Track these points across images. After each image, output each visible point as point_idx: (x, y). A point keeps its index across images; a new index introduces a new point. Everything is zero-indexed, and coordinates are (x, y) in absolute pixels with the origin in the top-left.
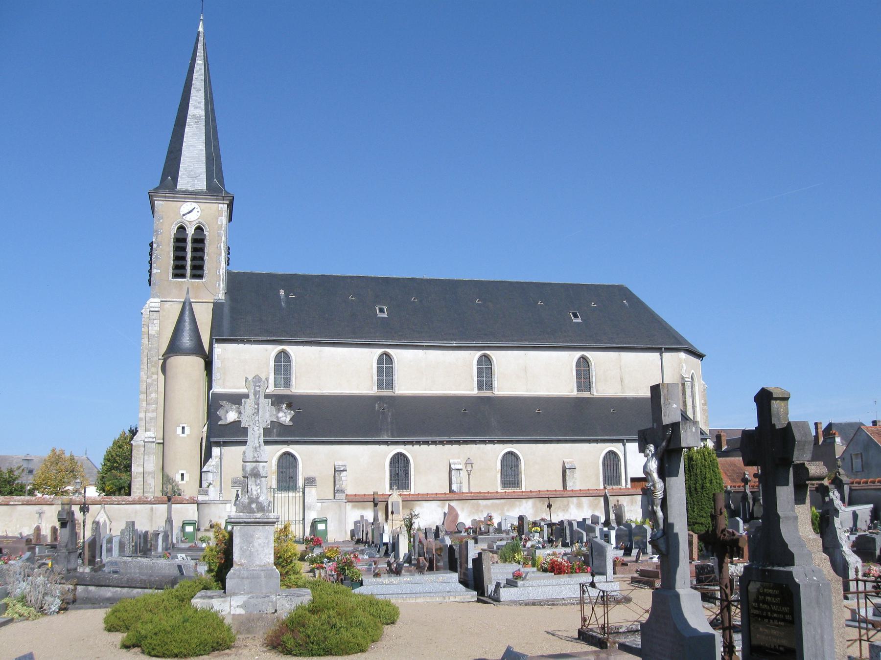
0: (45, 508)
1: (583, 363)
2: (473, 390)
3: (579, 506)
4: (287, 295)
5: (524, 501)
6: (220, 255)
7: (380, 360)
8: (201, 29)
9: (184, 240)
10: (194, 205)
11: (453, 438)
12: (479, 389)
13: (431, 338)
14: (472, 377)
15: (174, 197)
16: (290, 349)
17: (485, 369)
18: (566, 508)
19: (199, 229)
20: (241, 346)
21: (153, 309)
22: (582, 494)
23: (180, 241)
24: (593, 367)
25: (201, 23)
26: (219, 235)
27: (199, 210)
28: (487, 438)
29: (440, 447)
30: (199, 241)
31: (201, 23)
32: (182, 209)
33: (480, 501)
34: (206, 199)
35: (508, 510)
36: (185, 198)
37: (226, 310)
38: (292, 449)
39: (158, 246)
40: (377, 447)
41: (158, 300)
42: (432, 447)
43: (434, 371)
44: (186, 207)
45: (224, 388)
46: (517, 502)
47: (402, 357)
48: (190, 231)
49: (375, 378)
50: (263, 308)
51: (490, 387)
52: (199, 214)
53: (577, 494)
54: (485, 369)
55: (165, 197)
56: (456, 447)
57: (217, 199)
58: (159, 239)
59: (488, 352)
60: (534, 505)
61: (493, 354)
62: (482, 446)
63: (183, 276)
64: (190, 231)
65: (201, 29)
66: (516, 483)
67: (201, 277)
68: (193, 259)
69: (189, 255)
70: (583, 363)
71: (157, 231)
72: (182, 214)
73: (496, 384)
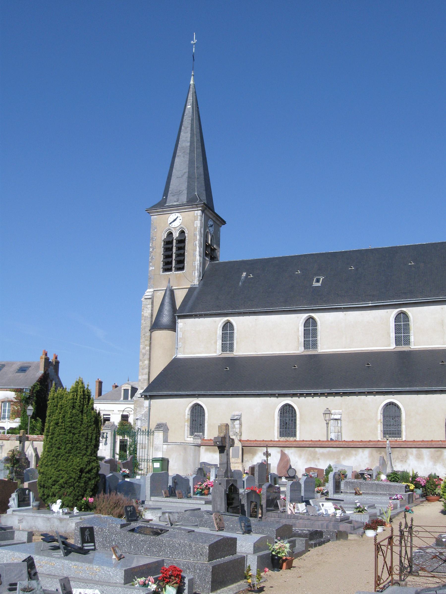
0: (5, 442)
1: (228, 327)
2: (389, 345)
3: (419, 457)
4: (247, 275)
5: (360, 450)
6: (196, 251)
7: (397, 318)
8: (192, 82)
9: (171, 243)
10: (178, 215)
11: (334, 390)
12: (396, 344)
13: (352, 300)
14: (389, 334)
15: (163, 211)
16: (233, 320)
17: (402, 326)
18: (404, 459)
19: (182, 232)
20: (197, 320)
21: (146, 297)
22: (422, 444)
23: (168, 243)
24: (319, 327)
25: (192, 77)
26: (195, 235)
27: (181, 218)
28: (312, 391)
29: (323, 398)
30: (182, 241)
31: (192, 77)
32: (169, 219)
33: (317, 449)
34: (185, 209)
35: (344, 459)
36: (171, 210)
37: (195, 293)
38: (201, 401)
39: (153, 250)
40: (268, 399)
41: (152, 290)
42: (316, 398)
43: (355, 330)
44: (172, 217)
45: (184, 354)
46: (353, 451)
47: (324, 319)
48: (176, 235)
49: (302, 339)
50: (230, 288)
51: (407, 342)
52: (181, 221)
53: (417, 445)
54: (402, 326)
55: (158, 212)
56: (338, 398)
57: (193, 208)
58: (154, 244)
59: (404, 309)
60: (371, 455)
61: (410, 311)
62: (363, 397)
63: (170, 270)
64: (176, 235)
65: (192, 82)
66: (398, 433)
67: (182, 269)
68: (178, 255)
69: (174, 254)
70: (228, 327)
71: (153, 238)
72: (169, 222)
73: (412, 339)
